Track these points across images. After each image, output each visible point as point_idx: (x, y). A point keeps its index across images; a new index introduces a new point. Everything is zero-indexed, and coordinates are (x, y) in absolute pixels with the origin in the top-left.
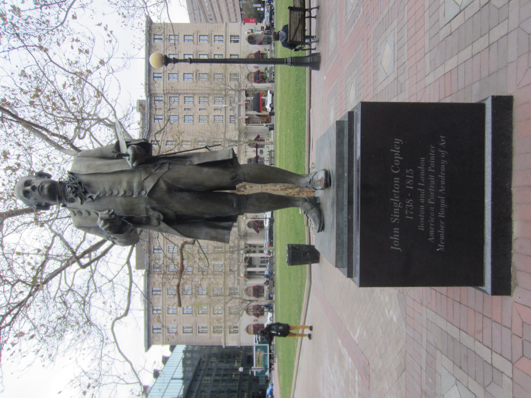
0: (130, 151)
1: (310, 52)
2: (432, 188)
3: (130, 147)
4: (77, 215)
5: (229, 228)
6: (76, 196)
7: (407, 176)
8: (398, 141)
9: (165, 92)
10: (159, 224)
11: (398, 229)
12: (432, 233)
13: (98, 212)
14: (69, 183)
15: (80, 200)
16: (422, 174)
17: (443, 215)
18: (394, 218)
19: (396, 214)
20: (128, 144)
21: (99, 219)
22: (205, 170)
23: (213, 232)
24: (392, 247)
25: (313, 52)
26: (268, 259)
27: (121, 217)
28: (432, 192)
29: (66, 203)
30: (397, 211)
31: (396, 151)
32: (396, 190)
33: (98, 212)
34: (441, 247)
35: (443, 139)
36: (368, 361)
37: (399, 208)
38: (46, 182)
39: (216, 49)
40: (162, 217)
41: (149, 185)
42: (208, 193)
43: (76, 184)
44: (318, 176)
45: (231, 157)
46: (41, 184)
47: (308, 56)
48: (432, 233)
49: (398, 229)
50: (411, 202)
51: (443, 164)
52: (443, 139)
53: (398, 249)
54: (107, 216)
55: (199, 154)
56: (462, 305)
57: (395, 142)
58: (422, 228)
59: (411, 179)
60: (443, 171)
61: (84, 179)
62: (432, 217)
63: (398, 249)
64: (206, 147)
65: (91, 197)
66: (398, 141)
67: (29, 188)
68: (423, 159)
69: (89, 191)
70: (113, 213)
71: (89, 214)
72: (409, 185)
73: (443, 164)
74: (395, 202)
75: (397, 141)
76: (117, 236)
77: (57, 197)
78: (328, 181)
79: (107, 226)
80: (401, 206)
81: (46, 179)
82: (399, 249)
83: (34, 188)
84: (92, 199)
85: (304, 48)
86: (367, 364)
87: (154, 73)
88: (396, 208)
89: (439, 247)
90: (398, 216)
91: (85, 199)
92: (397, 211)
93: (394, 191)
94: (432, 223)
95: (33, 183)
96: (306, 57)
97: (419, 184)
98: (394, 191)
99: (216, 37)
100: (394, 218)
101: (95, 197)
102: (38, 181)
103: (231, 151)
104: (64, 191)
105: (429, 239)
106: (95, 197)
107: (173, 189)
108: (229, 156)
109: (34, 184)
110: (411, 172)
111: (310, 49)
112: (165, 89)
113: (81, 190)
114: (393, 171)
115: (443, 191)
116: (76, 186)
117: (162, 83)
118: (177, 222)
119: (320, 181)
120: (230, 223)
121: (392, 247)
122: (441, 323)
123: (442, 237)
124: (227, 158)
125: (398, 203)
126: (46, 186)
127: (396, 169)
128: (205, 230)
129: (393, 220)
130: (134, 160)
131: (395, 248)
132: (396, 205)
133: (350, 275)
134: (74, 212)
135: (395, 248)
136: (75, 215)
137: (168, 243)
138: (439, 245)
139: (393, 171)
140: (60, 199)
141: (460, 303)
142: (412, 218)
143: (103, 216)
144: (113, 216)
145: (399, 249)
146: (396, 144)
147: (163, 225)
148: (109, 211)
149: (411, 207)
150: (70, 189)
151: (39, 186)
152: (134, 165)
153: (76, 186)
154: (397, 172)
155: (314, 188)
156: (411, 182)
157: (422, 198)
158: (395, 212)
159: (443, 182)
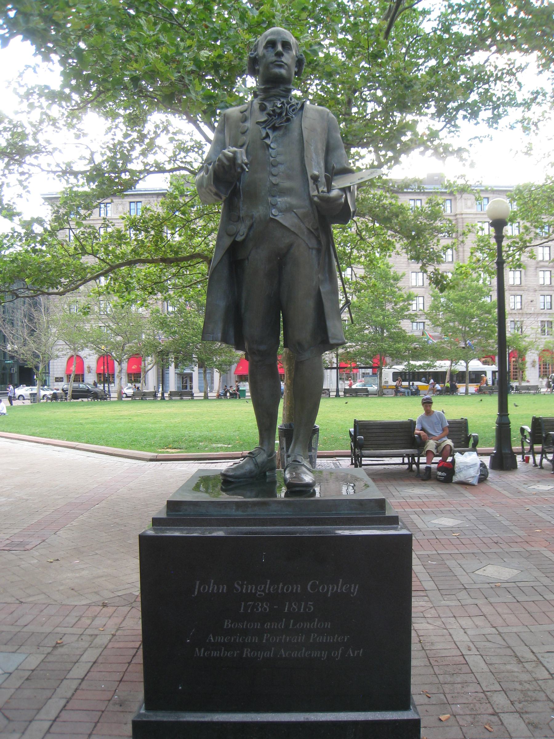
0: (335, 193)
1: (519, 453)
2: (286, 639)
3: (340, 193)
4: (241, 115)
5: (224, 340)
6: (269, 115)
7: (303, 603)
8: (354, 590)
9: (458, 216)
10: (230, 235)
11: (225, 591)
12: (221, 639)
13: (245, 147)
14: (288, 103)
15: (263, 120)
16: (307, 625)
17: (247, 654)
18: (242, 586)
19: (247, 589)
20: (346, 190)
21: (235, 149)
22: (311, 304)
23: (219, 315)
24: (198, 583)
25: (519, 458)
26: (188, 389)
27: (239, 180)
28: (281, 640)
29: (259, 97)
30: (251, 590)
31: (340, 587)
32: (283, 588)
33: (245, 147)
34: (201, 652)
35: (358, 653)
36: (32, 549)
37: (256, 593)
38: (289, 70)
39: (530, 298)
40: (239, 239)
41: (286, 220)
42: (278, 305)
43: (286, 115)
44: (305, 473)
45: (332, 341)
46: (286, 64)
47: (511, 450)
48: (221, 639)
49: (225, 591)
50: (265, 609)
51: (321, 653)
52: (358, 653)
53: (196, 590)
54: (239, 162)
55: (335, 292)
56: (117, 683)
57: (353, 585)
58: (227, 624)
59: (299, 609)
60: (311, 654)
61: (295, 125)
62: (243, 640)
63: (196, 590)
64: (347, 302)
65: (267, 136)
66: (355, 589)
67: (280, 48)
68: (328, 625)
69: (276, 133)
70: (243, 169)
71: (243, 133)
72: (290, 606)
73: (321, 653)
74: (265, 587)
75: (355, 588)
76: (210, 175)
77: (268, 86)
78: (297, 489)
79: (225, 161)
80: (259, 595)
81: (294, 69)
82: (196, 593)
83: (279, 55)
84: (265, 138)
85: (525, 443)
86: (28, 547)
87: (488, 198)
88: (256, 589)
89: (200, 650)
90: (244, 591)
91: (265, 128)
92: (251, 590)
93: (281, 585)
94: (235, 640)
95: (288, 53)
96: (511, 447)
97: (292, 621)
98: (281, 585)
99: (549, 297)
100: (242, 586)
101: (268, 141)
102: (290, 60)
103: (340, 342)
104: (278, 96)
105: (211, 635)
106: (268, 141)
107: (281, 261)
108: (334, 339)
109: (285, 54)
110: (310, 609)
111: (522, 453)
112: (464, 216)
113: (278, 121)
114: (310, 583)
115: (281, 655)
116: (284, 114)
117: (474, 211)
118: (232, 262)
119: (298, 476)
120: (233, 340)
121: (198, 583)
122: (90, 656)
123: (215, 654)
124: (330, 335)
125: (264, 591)
126: (283, 71)
127: (314, 587)
128: (222, 304)
129: (238, 584)
130: (321, 198)
131: (197, 587)
132: (261, 588)
133: (156, 522)
134: (245, 111)
135: (197, 587)
136: (242, 112)
137: (206, 234)
138: (202, 650)
139: (310, 583)
140: (265, 91)
141: (120, 681)
142: (242, 611)
143: (239, 155)
144: (239, 170)
145: (196, 593)
146: (350, 587)
147: (227, 242)
148: (246, 164)
149: (258, 609)
150: (279, 106)
151: (282, 62)
152: (316, 199)
153: (284, 114)
154: (309, 589)
155: (287, 467)
156: (294, 609)
157: (271, 625)
158: (250, 587)
159: (295, 654)
